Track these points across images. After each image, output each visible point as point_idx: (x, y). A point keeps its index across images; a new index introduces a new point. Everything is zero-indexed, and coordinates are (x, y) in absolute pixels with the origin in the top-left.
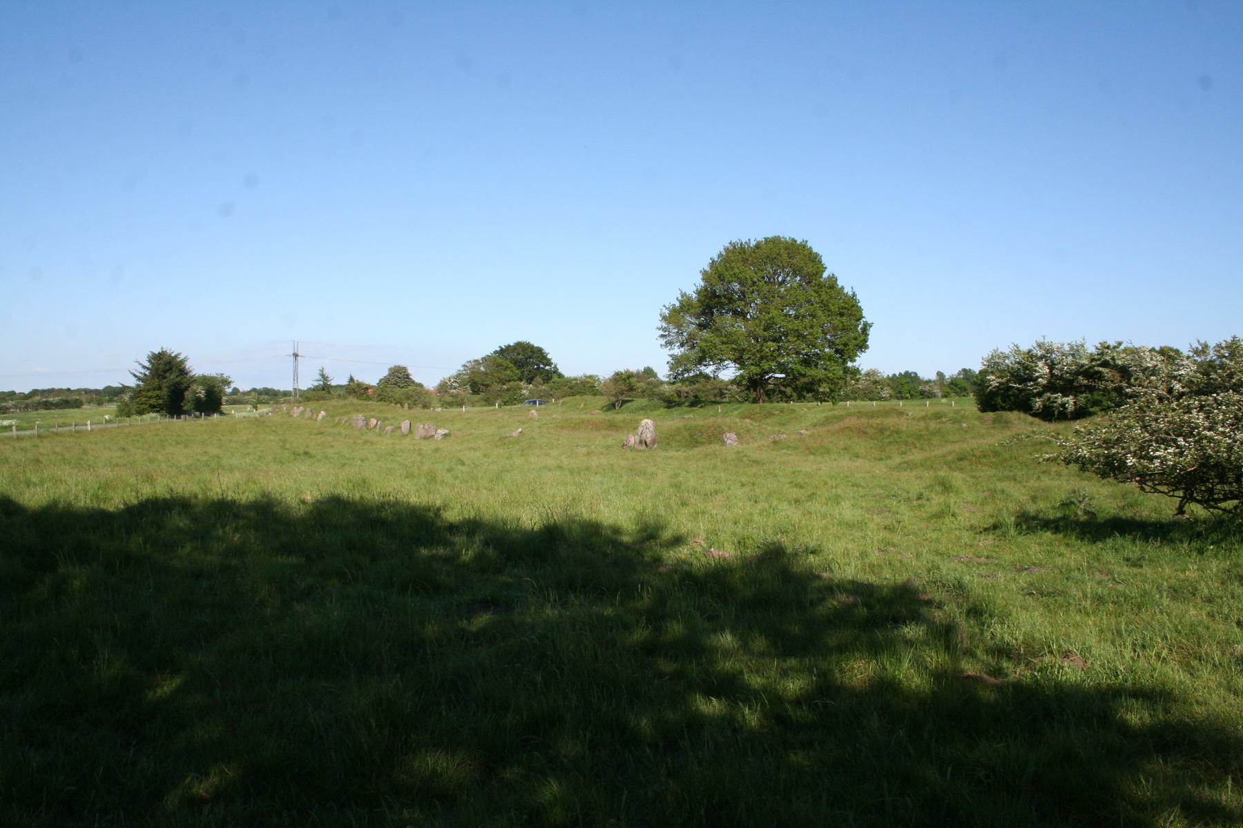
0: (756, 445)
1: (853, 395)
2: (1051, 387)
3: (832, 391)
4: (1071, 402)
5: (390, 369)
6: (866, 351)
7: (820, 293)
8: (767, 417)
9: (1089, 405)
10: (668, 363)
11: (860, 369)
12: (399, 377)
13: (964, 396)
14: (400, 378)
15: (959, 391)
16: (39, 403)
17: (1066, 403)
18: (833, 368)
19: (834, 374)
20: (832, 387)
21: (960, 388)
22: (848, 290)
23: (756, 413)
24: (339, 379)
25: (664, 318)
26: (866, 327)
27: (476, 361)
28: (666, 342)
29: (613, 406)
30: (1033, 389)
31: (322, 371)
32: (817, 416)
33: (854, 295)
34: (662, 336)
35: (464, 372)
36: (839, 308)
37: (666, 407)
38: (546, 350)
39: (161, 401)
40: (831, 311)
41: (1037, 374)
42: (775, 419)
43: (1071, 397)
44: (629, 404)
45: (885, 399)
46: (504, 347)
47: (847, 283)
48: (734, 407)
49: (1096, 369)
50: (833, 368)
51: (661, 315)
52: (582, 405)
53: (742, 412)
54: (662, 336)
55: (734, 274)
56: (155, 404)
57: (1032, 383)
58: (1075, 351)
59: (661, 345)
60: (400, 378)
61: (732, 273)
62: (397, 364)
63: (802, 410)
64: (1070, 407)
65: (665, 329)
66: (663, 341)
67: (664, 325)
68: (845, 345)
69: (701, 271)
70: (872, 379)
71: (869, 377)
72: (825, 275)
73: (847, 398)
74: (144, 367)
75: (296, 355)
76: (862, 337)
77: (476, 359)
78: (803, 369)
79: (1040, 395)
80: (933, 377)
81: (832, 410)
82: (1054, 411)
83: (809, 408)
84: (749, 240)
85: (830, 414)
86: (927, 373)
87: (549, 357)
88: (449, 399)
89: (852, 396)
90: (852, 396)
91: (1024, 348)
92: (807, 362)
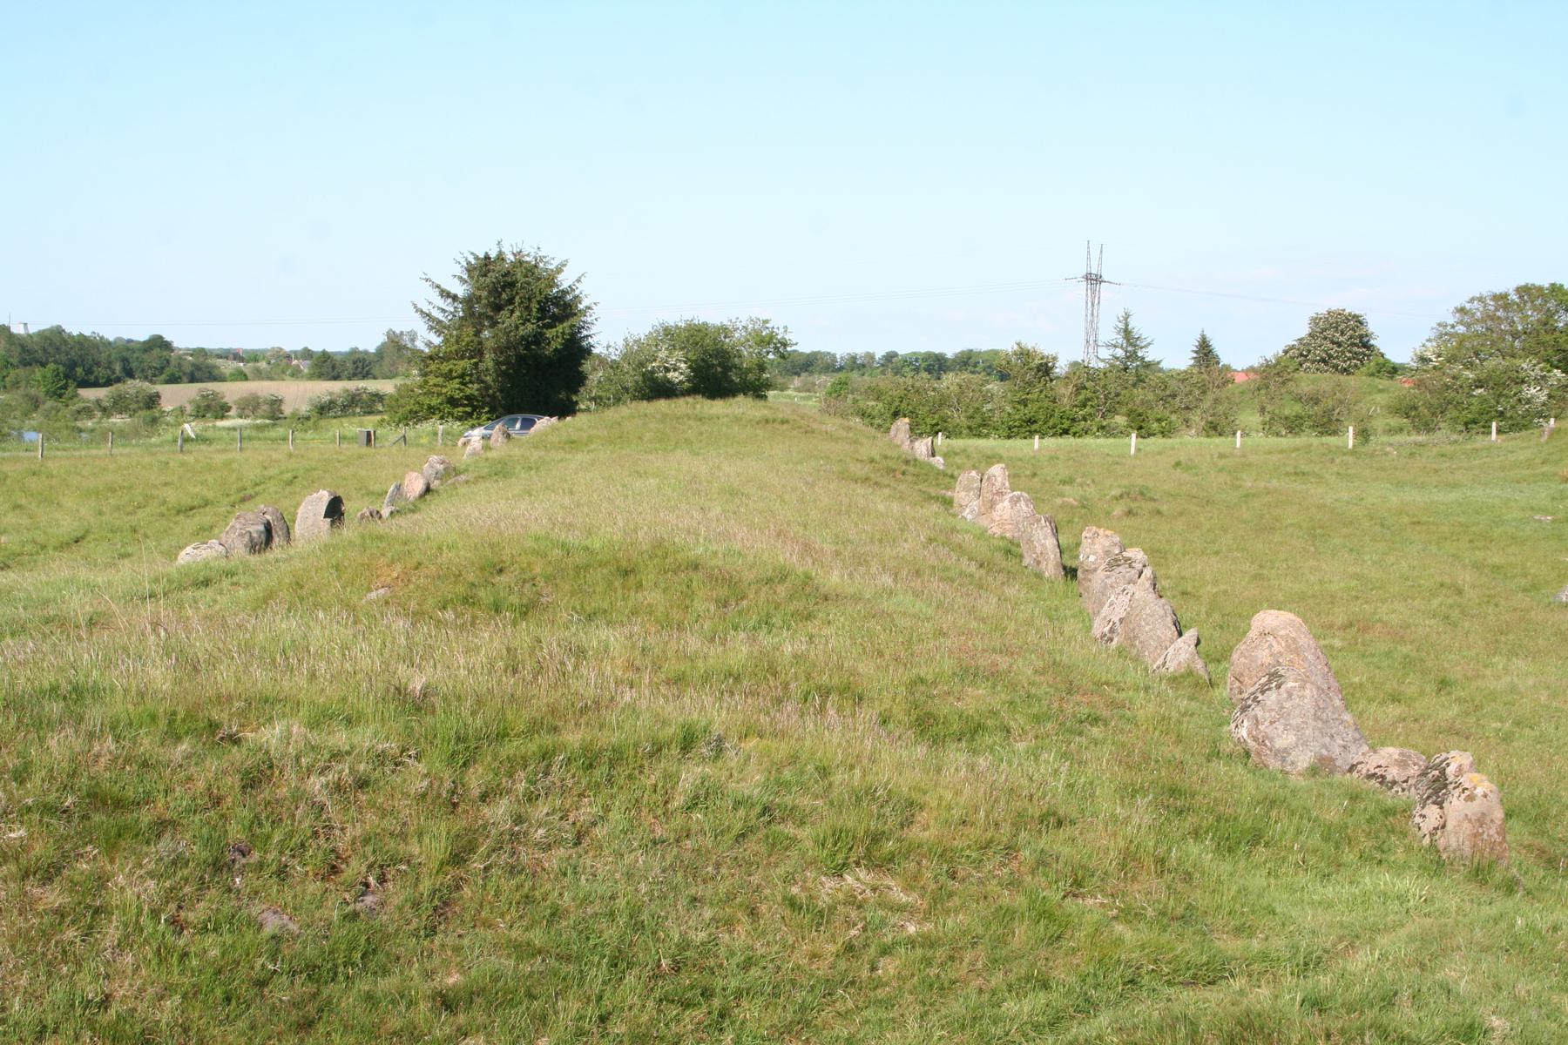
5: (1315, 321)
14: (1339, 345)
27: (1501, 298)
31: (1127, 316)
39: (473, 389)
56: (457, 395)
60: (1339, 345)
74: (445, 294)
75: (1094, 280)
88: (1292, 409)
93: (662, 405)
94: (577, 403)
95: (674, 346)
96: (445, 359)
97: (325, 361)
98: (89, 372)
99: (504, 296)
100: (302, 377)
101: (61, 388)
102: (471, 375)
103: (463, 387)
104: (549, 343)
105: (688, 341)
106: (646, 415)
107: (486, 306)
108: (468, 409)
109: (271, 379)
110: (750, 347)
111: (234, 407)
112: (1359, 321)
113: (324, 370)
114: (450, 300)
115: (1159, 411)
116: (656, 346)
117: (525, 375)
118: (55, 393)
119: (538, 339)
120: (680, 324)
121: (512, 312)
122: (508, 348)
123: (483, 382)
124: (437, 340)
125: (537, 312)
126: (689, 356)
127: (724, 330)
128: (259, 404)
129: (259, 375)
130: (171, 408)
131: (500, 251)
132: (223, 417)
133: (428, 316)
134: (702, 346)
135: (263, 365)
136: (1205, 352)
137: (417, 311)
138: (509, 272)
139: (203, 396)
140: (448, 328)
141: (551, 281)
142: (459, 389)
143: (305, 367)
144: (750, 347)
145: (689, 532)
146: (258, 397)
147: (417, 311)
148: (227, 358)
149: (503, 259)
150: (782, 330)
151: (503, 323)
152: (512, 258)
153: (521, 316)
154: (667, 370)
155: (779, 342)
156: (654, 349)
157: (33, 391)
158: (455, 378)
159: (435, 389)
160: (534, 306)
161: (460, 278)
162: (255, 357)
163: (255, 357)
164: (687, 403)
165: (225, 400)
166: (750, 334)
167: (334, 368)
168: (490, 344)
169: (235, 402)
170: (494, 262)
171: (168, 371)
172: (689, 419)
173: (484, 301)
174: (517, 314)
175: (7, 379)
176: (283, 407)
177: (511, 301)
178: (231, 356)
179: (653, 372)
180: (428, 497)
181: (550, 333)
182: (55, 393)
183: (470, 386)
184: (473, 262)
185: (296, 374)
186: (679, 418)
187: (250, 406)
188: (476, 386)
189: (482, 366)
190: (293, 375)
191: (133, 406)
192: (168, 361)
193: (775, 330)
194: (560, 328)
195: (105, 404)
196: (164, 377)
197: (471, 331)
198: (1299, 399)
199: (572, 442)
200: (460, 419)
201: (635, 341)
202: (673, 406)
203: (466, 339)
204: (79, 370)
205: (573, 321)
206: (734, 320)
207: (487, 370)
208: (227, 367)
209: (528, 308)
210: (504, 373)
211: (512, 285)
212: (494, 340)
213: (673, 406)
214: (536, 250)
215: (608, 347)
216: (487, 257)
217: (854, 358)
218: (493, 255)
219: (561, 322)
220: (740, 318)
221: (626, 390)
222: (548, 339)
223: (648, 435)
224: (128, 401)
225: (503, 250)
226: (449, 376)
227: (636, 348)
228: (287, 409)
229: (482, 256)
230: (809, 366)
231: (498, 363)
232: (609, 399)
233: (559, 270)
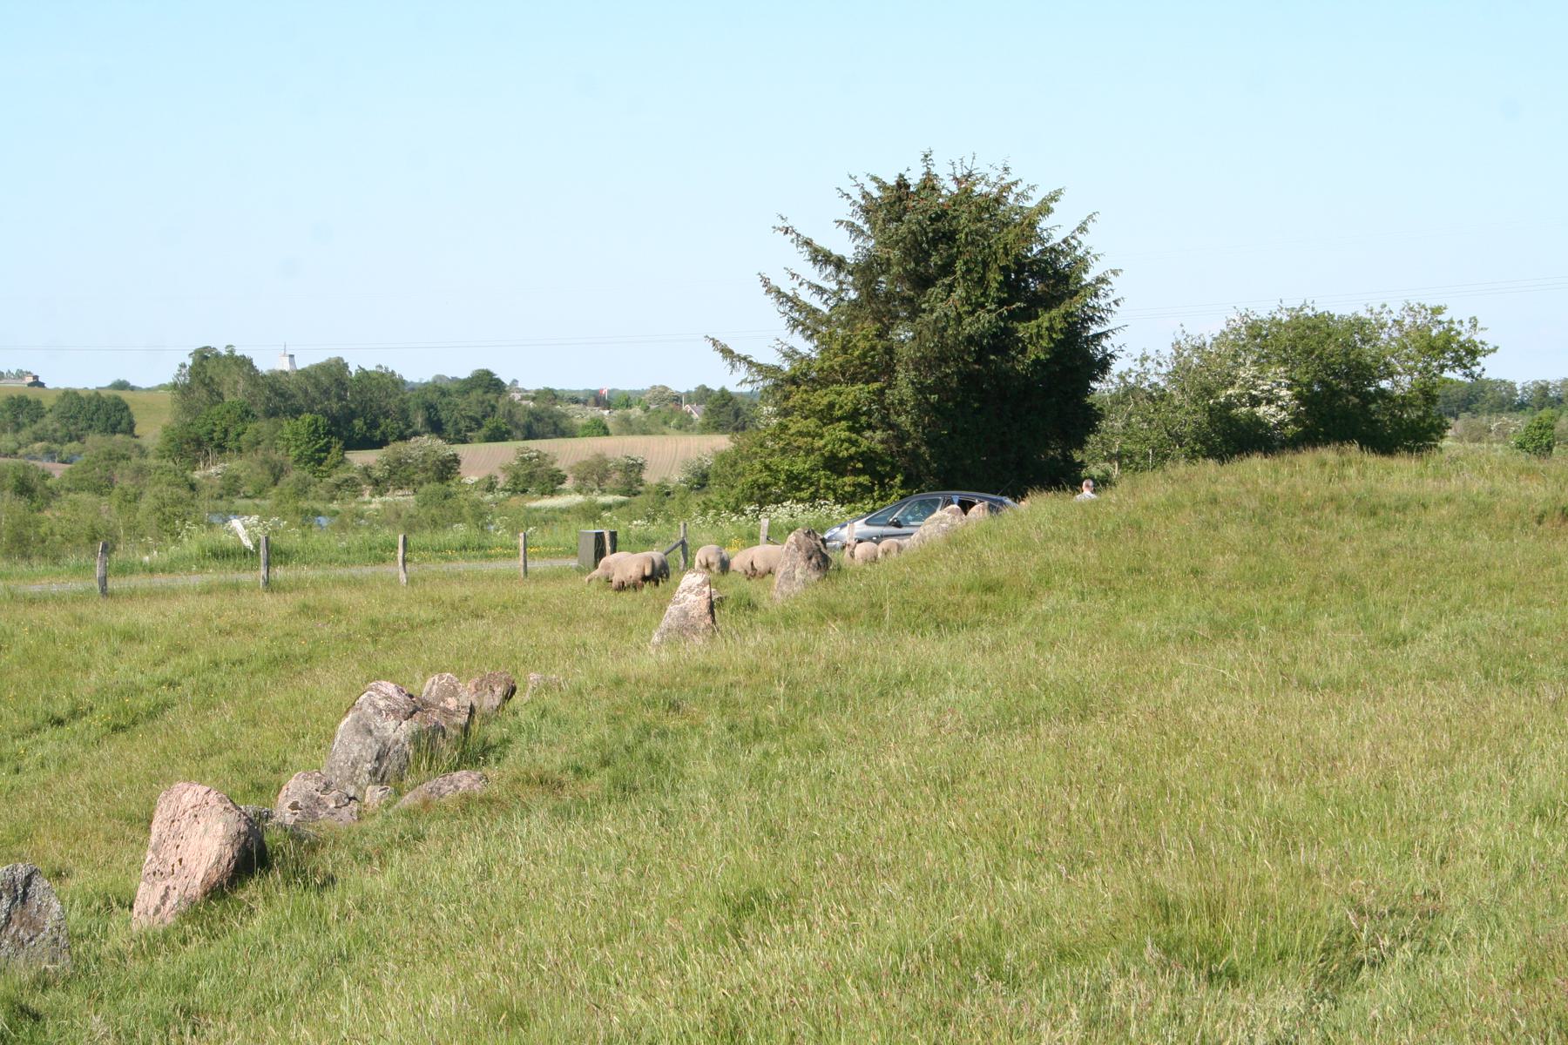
39: (874, 440)
74: (822, 257)
93: (1256, 466)
94: (1082, 465)
95: (1267, 356)
96: (823, 382)
97: (726, 405)
98: (374, 425)
99: (935, 259)
100: (693, 429)
101: (320, 450)
102: (869, 413)
103: (854, 436)
104: (1024, 351)
105: (1294, 348)
106: (1214, 501)
107: (900, 278)
108: (864, 479)
109: (645, 433)
110: (1409, 358)
111: (570, 476)
113: (723, 418)
114: (830, 269)
116: (1236, 355)
117: (978, 411)
118: (311, 458)
119: (1002, 341)
120: (1278, 316)
121: (950, 288)
122: (943, 359)
123: (892, 426)
124: (805, 347)
125: (998, 290)
126: (1296, 374)
127: (1359, 325)
128: (607, 470)
129: (628, 427)
130: (476, 479)
131: (928, 173)
132: (553, 493)
133: (793, 302)
134: (1320, 357)
135: (636, 412)
137: (768, 292)
138: (945, 213)
139: (523, 460)
140: (828, 321)
141: (1028, 227)
142: (849, 440)
143: (696, 413)
144: (1409, 358)
146: (606, 461)
147: (768, 292)
148: (585, 403)
149: (933, 188)
150: (1467, 325)
151: (932, 311)
152: (954, 188)
153: (968, 299)
154: (1256, 402)
155: (1462, 346)
156: (1230, 363)
157: (277, 457)
158: (839, 420)
159: (801, 441)
160: (994, 277)
161: (852, 227)
162: (628, 400)
163: (628, 400)
164: (1323, 464)
165: (557, 466)
166: (1407, 335)
167: (737, 415)
168: (906, 352)
169: (571, 469)
170: (918, 193)
171: (489, 423)
172: (1340, 509)
173: (895, 269)
174: (960, 292)
175: (242, 437)
176: (645, 476)
177: (947, 269)
178: (592, 400)
179: (1229, 405)
180: (252, 890)
181: (1024, 330)
182: (311, 458)
183: (868, 433)
184: (876, 194)
185: (685, 425)
186: (1309, 508)
187: (595, 474)
188: (879, 435)
189: (891, 396)
190: (679, 427)
191: (419, 477)
192: (493, 408)
193: (1456, 326)
194: (1044, 319)
195: (377, 474)
196: (484, 431)
197: (871, 328)
199: (989, 589)
200: (841, 500)
201: (1196, 349)
202: (1285, 471)
203: (862, 344)
204: (358, 423)
205: (1074, 305)
206: (1376, 310)
207: (902, 402)
208: (582, 416)
209: (982, 281)
210: (936, 408)
211: (950, 237)
212: (915, 344)
213: (1285, 471)
214: (1000, 172)
215: (1144, 359)
216: (902, 184)
217: (1543, 389)
218: (915, 179)
219: (1048, 308)
220: (1390, 306)
221: (1179, 439)
222: (1020, 340)
223: (1222, 565)
224: (412, 469)
225: (934, 170)
226: (827, 416)
227: (1196, 361)
228: (650, 477)
229: (891, 181)
230: (1471, 402)
231: (921, 389)
232: (1146, 457)
233: (1044, 209)
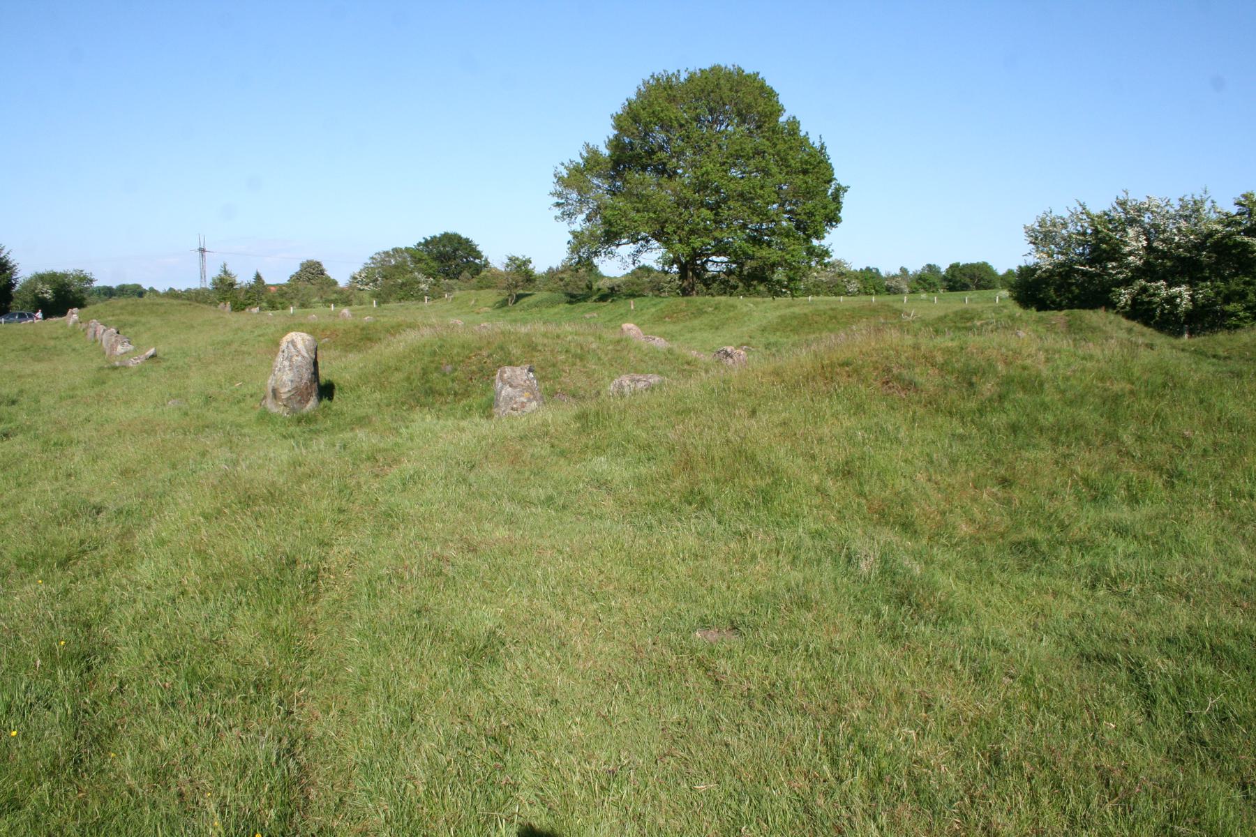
0: (365, 597)
1: (815, 289)
2: (1148, 271)
3: (791, 279)
4: (1186, 295)
5: (302, 265)
6: (838, 225)
7: (775, 140)
8: (695, 317)
9: (1220, 300)
10: (569, 242)
11: (830, 250)
12: (312, 272)
13: (933, 292)
14: (313, 274)
15: (927, 286)
16: (541, 302)
17: (1177, 297)
18: (792, 248)
19: (793, 256)
20: (791, 274)
21: (929, 284)
22: (814, 140)
23: (681, 311)
24: (244, 278)
25: (560, 180)
26: (840, 190)
27: (387, 253)
28: (563, 214)
29: (504, 304)
30: (1117, 273)
31: (225, 265)
32: (768, 315)
33: (823, 147)
34: (558, 205)
35: (372, 265)
36: (801, 162)
37: (567, 302)
38: (476, 242)
40: (790, 166)
41: (1127, 249)
42: (705, 320)
43: (1184, 288)
44: (526, 299)
45: (853, 294)
46: (429, 239)
47: (813, 130)
48: (653, 302)
49: (1238, 238)
50: (792, 248)
51: (555, 176)
52: (473, 302)
53: (661, 309)
54: (558, 205)
55: (653, 112)
57: (1114, 264)
58: (1192, 211)
59: (556, 218)
60: (313, 274)
61: (651, 111)
62: (310, 258)
63: (746, 305)
64: (1185, 303)
65: (559, 195)
66: (558, 212)
67: (559, 189)
68: (810, 214)
69: (612, 116)
70: (837, 270)
71: (834, 268)
72: (782, 119)
73: (807, 292)
75: (202, 251)
76: (833, 206)
77: (386, 250)
78: (751, 249)
79: (1127, 282)
80: (898, 272)
81: (789, 306)
82: (1155, 310)
83: (756, 304)
84: (679, 71)
85: (788, 311)
86: (888, 268)
87: (479, 248)
89: (814, 290)
90: (814, 290)
91: (1096, 209)
92: (756, 241)
112: (319, 264)
115: (279, 300)
136: (258, 277)
145: (464, 347)
198: (336, 292)
